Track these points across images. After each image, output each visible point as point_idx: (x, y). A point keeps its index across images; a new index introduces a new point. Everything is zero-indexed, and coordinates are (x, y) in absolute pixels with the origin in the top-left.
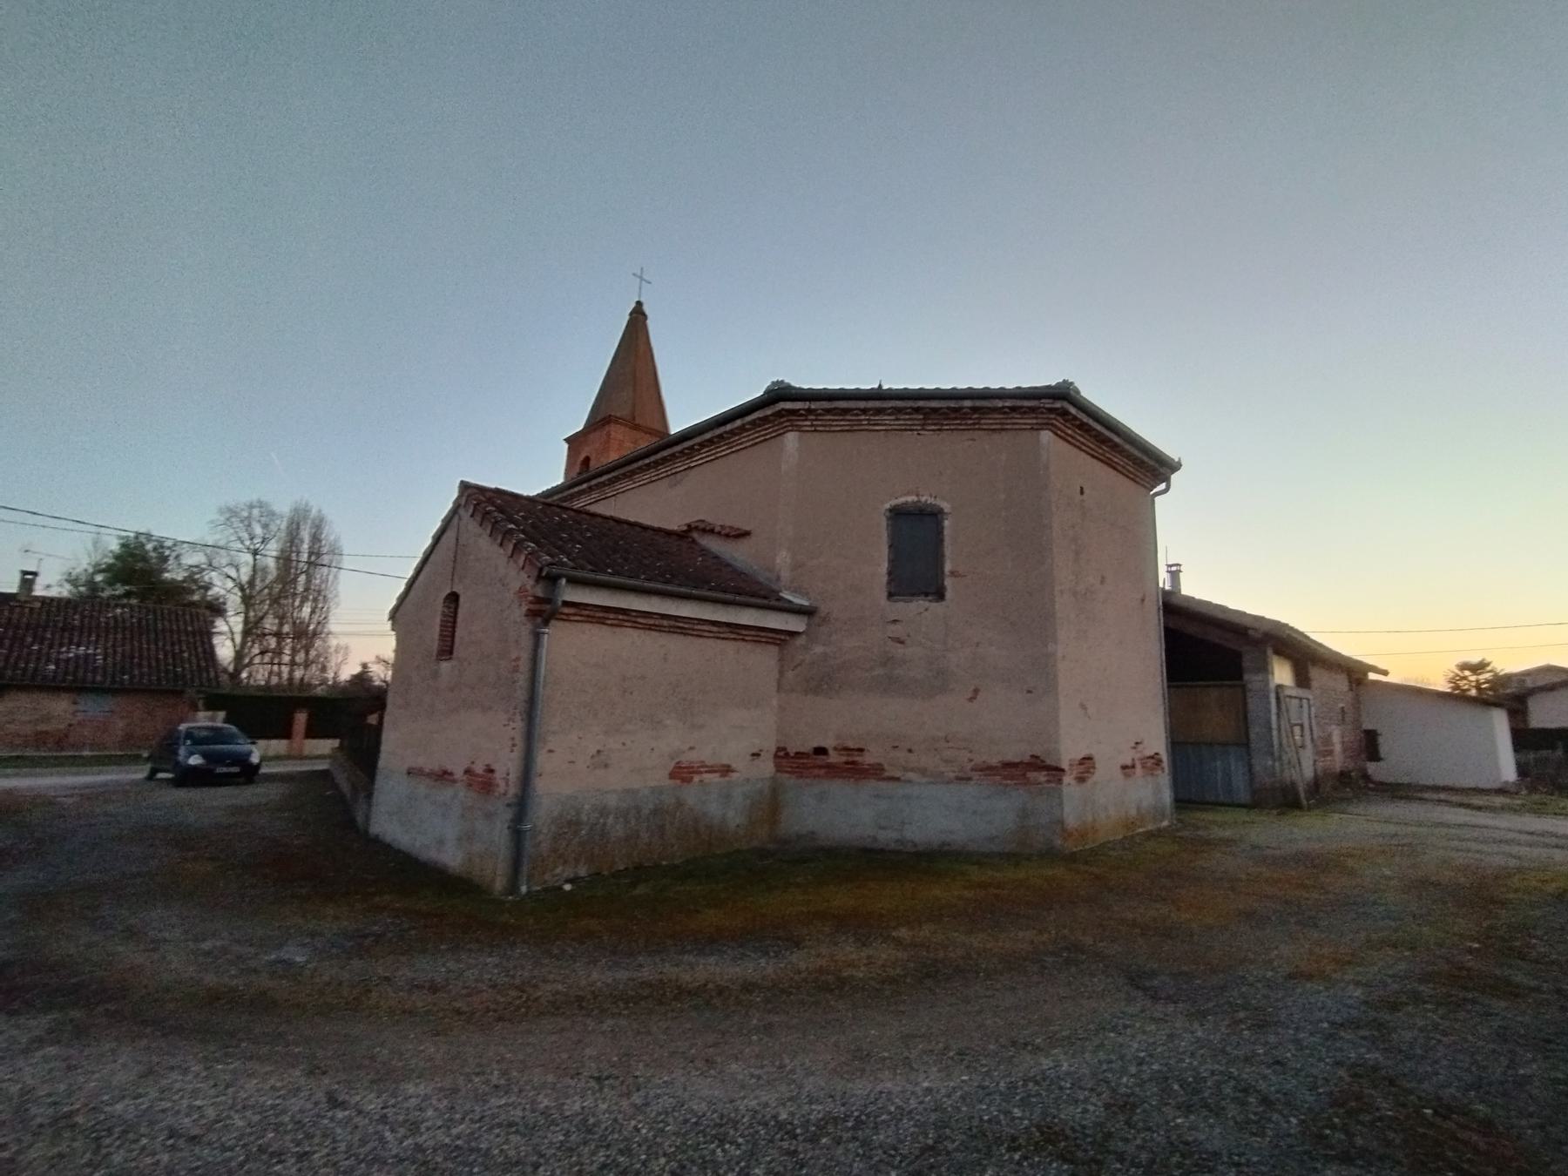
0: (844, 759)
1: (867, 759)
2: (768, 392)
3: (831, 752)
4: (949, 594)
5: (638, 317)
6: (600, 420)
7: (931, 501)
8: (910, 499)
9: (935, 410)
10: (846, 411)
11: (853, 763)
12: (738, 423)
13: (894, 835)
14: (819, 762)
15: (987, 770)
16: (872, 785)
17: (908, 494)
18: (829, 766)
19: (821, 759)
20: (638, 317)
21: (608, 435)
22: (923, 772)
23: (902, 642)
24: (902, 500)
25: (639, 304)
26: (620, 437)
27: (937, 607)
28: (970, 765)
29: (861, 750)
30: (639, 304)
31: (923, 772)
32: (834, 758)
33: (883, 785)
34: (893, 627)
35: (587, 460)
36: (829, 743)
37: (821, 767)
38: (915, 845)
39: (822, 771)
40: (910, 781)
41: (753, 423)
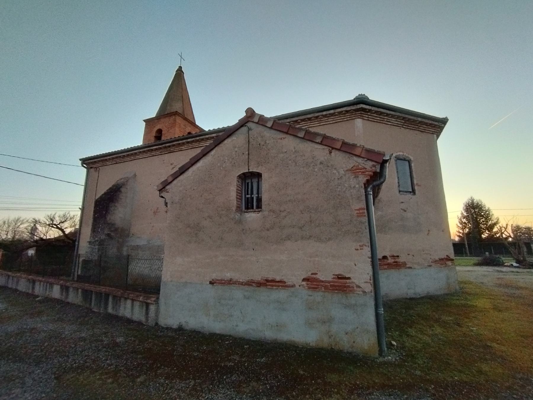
0: (393, 260)
1: (401, 260)
2: (357, 98)
3: (389, 258)
4: (417, 192)
5: (180, 73)
6: (165, 113)
7: (407, 155)
8: (401, 153)
9: (409, 119)
10: (381, 113)
11: (396, 262)
12: (332, 112)
13: (412, 291)
14: (385, 263)
15: (435, 261)
16: (403, 271)
17: (400, 151)
18: (388, 264)
19: (386, 261)
20: (180, 73)
21: (175, 120)
22: (418, 264)
23: (405, 211)
24: (398, 153)
25: (180, 67)
26: (180, 122)
27: (414, 197)
28: (431, 261)
29: (398, 256)
30: (180, 67)
31: (418, 264)
32: (390, 260)
33: (408, 270)
34: (402, 204)
35: (160, 131)
36: (387, 254)
37: (385, 265)
38: (420, 295)
39: (386, 267)
40: (415, 268)
41: (340, 113)
